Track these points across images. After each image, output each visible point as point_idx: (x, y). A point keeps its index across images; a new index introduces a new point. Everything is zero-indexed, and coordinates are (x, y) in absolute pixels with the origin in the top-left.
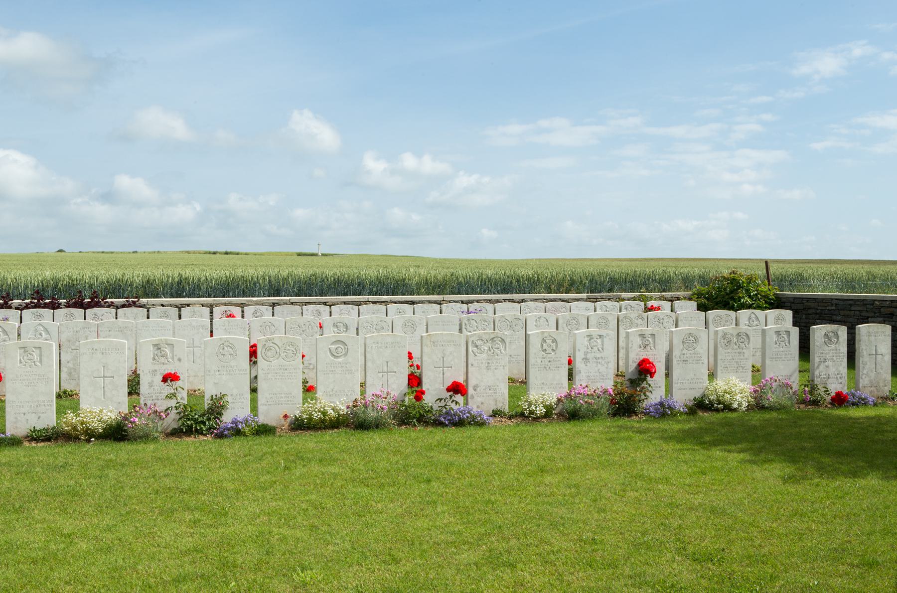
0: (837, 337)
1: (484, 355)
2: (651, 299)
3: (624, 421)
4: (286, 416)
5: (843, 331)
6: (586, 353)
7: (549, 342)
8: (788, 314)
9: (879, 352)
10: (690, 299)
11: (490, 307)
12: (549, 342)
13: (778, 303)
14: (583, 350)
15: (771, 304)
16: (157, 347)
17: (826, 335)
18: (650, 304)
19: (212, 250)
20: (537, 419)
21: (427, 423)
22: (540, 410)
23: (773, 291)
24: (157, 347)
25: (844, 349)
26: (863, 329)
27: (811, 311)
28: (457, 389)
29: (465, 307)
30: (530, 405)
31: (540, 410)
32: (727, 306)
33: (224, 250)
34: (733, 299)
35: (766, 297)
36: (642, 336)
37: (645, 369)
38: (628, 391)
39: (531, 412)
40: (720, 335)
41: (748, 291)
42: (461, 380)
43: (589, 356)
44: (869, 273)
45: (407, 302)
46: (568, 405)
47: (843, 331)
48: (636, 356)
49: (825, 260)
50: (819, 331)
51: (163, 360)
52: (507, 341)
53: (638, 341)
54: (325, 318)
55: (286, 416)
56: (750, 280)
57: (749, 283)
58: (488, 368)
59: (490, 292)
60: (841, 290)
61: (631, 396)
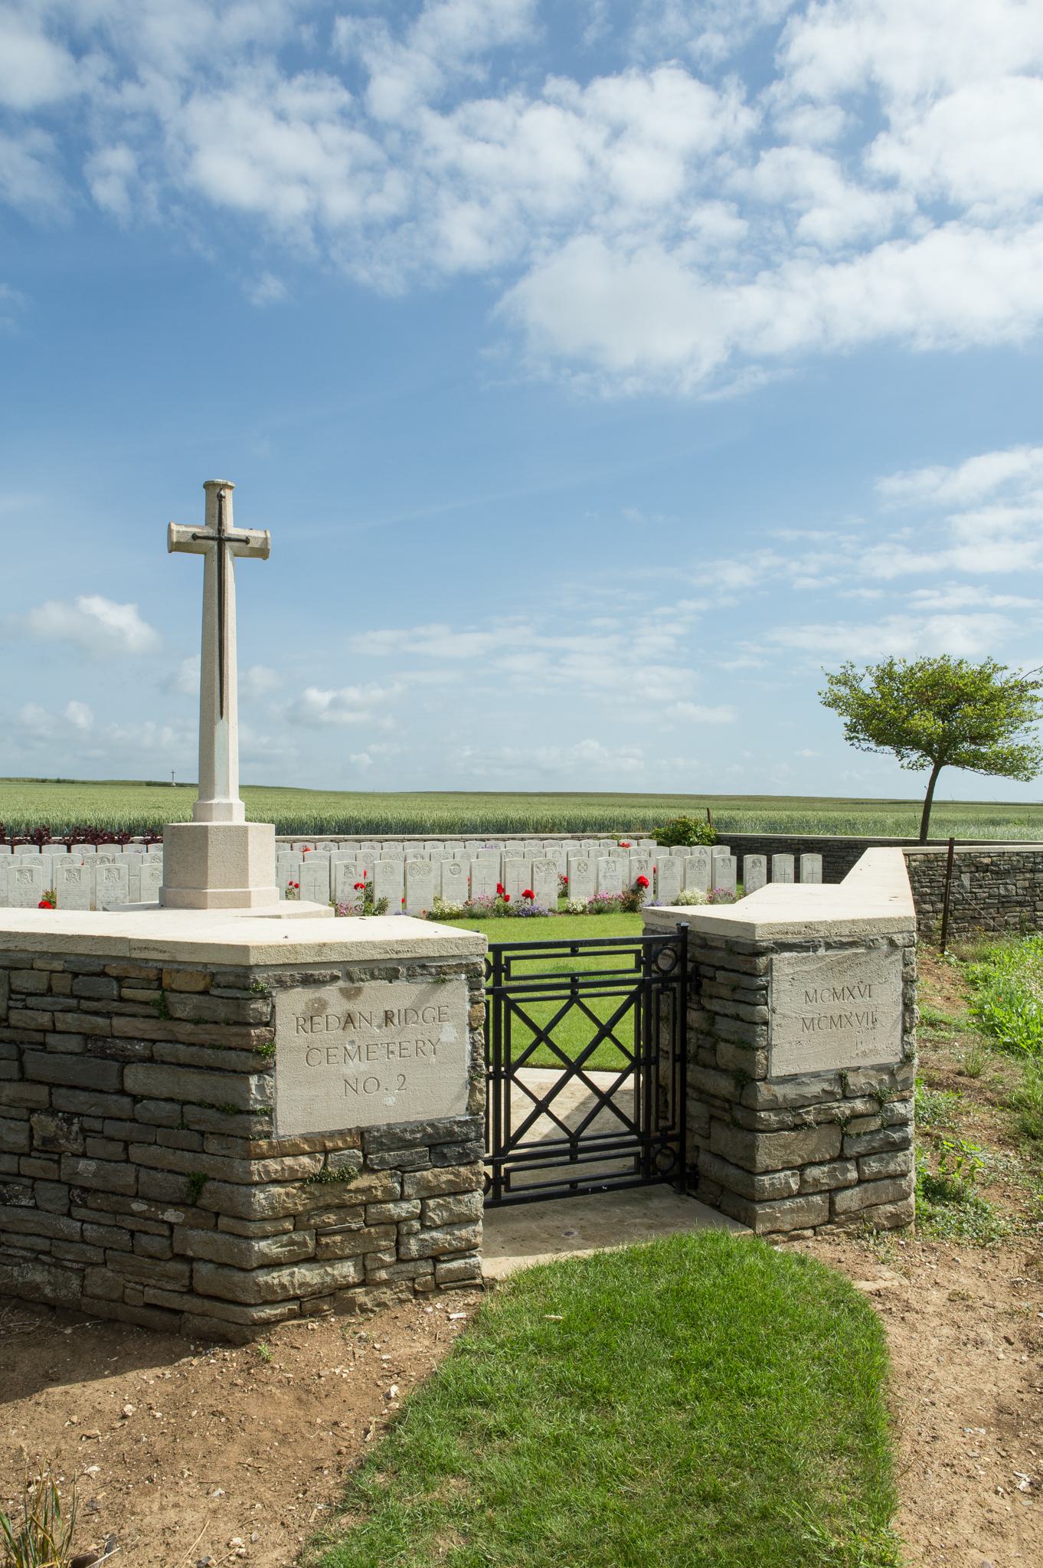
0: (760, 862)
1: (543, 874)
2: (621, 837)
3: (630, 915)
4: (424, 912)
5: (763, 858)
6: (605, 873)
7: (582, 865)
8: (728, 849)
9: (787, 872)
10: (650, 838)
11: (502, 843)
12: (582, 865)
13: (718, 841)
14: (604, 870)
15: (712, 842)
16: (347, 867)
17: (753, 862)
18: (622, 841)
19: (41, 777)
20: (577, 914)
21: (510, 916)
22: (580, 908)
23: (713, 832)
24: (347, 867)
25: (765, 871)
26: (776, 857)
27: (743, 847)
28: (528, 894)
29: (483, 843)
30: (573, 905)
31: (580, 908)
32: (679, 843)
33: (55, 778)
34: (685, 838)
35: (709, 836)
36: (639, 861)
37: (642, 883)
38: (632, 897)
39: (575, 909)
40: (688, 861)
41: (695, 832)
42: (529, 889)
43: (607, 874)
44: (788, 816)
45: (397, 840)
46: (595, 906)
47: (763, 858)
48: (636, 875)
49: (752, 796)
50: (749, 859)
51: (350, 875)
52: (557, 864)
53: (637, 865)
54: (335, 851)
55: (424, 912)
56: (697, 824)
57: (696, 826)
58: (545, 882)
59: (489, 832)
60: (766, 831)
61: (633, 901)
